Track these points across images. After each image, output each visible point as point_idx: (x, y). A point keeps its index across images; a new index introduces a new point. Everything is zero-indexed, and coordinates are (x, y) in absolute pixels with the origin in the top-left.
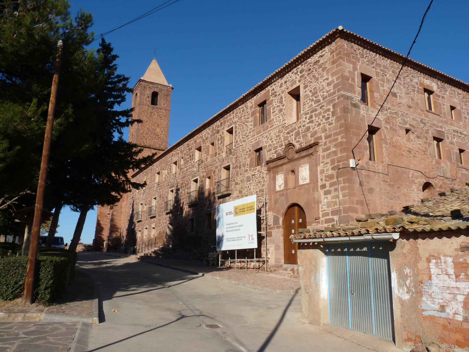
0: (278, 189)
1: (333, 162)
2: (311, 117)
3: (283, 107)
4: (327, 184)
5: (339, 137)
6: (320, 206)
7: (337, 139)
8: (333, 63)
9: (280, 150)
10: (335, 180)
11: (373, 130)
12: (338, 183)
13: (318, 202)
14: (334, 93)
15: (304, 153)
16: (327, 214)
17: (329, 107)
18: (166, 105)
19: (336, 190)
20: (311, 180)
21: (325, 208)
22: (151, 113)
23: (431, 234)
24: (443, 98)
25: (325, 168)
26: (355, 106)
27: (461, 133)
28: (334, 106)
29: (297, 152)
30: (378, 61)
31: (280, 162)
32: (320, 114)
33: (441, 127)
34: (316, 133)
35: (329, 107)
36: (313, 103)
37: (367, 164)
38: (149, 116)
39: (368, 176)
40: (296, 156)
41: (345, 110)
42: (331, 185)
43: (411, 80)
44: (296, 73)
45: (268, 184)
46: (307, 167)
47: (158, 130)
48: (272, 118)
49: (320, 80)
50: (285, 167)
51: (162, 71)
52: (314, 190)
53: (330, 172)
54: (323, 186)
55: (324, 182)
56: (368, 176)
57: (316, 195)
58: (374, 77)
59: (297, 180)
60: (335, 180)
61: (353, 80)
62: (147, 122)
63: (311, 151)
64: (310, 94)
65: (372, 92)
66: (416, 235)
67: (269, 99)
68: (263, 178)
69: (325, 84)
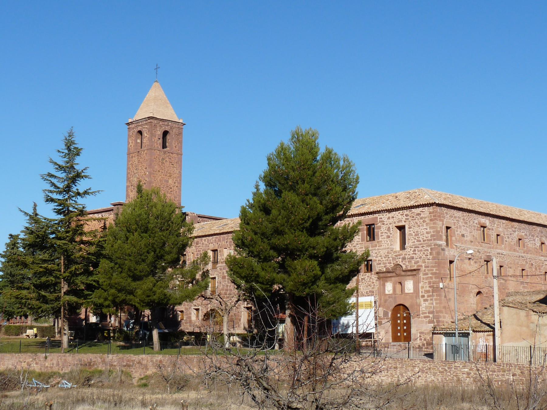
0: (387, 292)
1: (430, 283)
2: (415, 250)
3: (391, 235)
4: (426, 295)
5: (434, 269)
6: (421, 308)
7: (433, 270)
8: (431, 220)
9: (390, 266)
10: (431, 294)
11: (451, 262)
12: (433, 296)
13: (419, 305)
14: (431, 240)
15: (409, 273)
16: (426, 313)
17: (427, 248)
18: (177, 148)
19: (431, 300)
20: (414, 291)
21: (424, 309)
22: (163, 159)
23: (480, 331)
24: (492, 229)
25: (424, 286)
26: (443, 250)
27: (502, 254)
28: (431, 249)
29: (404, 271)
30: (456, 215)
31: (389, 275)
32: (421, 250)
33: (490, 253)
34: (418, 262)
35: (427, 248)
36: (416, 241)
37: (448, 284)
38: (161, 164)
39: (448, 291)
40: (403, 273)
41: (437, 252)
42: (428, 296)
43: (474, 222)
44: (402, 215)
45: (378, 288)
46: (412, 282)
47: (170, 181)
48: (380, 240)
49: (421, 228)
50: (393, 279)
51: (169, 100)
52: (416, 297)
53: (428, 289)
54: (423, 296)
55: (424, 294)
56: (448, 291)
57: (418, 301)
58: (453, 227)
59: (402, 290)
60: (431, 294)
61: (442, 232)
62: (159, 171)
63: (414, 273)
64: (414, 234)
65: (451, 236)
66: (476, 331)
67: (377, 224)
68: (373, 283)
69: (425, 231)
